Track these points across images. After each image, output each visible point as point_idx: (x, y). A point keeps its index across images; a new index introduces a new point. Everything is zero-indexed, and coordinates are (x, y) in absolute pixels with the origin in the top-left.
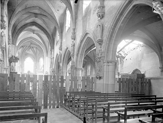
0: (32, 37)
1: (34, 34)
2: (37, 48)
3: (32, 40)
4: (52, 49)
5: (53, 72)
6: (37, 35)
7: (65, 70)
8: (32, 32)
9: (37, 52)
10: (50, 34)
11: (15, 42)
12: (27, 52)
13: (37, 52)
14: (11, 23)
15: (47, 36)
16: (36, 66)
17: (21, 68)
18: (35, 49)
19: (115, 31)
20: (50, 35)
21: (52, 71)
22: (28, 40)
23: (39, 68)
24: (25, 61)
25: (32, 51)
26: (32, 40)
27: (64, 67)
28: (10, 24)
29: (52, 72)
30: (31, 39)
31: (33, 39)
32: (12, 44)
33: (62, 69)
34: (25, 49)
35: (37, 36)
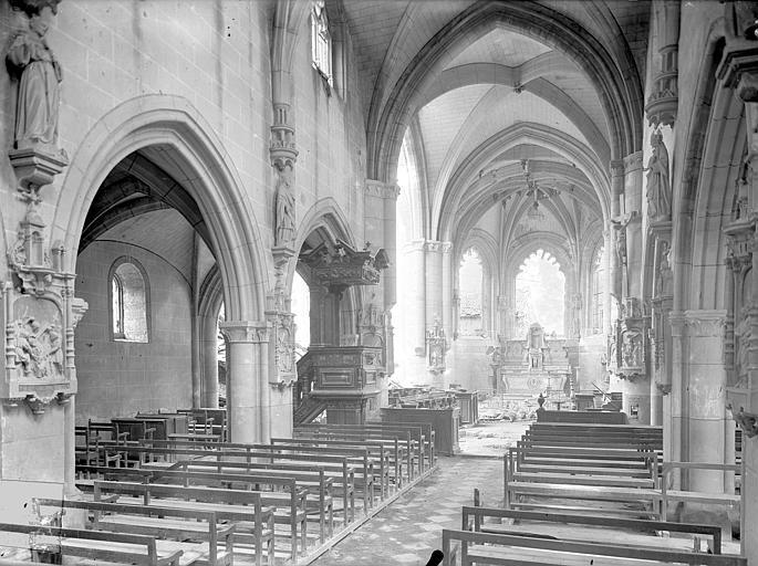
0: (527, 124)
1: (519, 90)
2: (572, 188)
3: (525, 140)
4: (624, 155)
5: (631, 323)
6: (540, 94)
7: (709, 302)
8: (506, 83)
9: (579, 213)
10: (600, 31)
11: (385, 164)
12: (527, 225)
13: (579, 213)
14: (280, 23)
15: (587, 68)
16: (579, 298)
17: (499, 314)
18: (565, 197)
19: (705, 507)
20: (611, 51)
21: (625, 316)
22: (503, 144)
23: (598, 306)
24: (518, 276)
25: (555, 212)
26: (525, 140)
27: (696, 273)
28: (280, 27)
29: (624, 327)
30: (518, 136)
31: (530, 135)
32: (369, 177)
33: (681, 292)
34: (512, 210)
35: (545, 101)
